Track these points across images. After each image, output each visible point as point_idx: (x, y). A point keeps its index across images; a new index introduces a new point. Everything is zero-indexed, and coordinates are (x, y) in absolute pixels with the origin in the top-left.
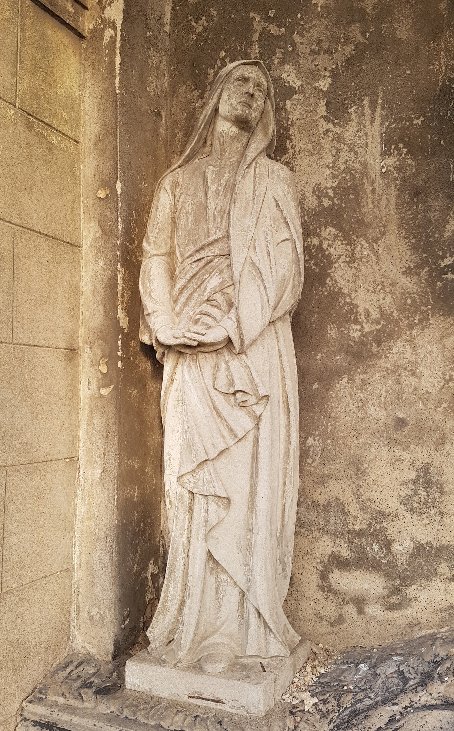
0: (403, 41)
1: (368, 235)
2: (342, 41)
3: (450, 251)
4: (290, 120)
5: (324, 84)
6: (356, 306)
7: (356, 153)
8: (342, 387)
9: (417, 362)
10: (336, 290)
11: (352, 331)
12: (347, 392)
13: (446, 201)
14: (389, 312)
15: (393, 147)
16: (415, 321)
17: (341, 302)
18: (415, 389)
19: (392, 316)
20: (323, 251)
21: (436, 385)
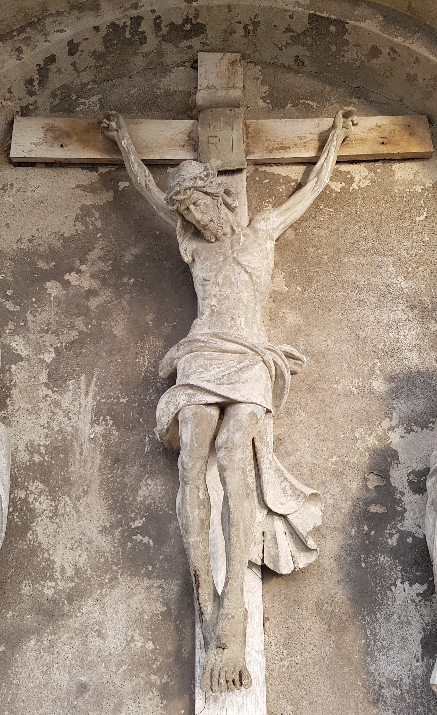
0: (117, 337)
1: (72, 493)
2: (68, 326)
3: (140, 514)
4: (13, 382)
5: (49, 357)
6: (53, 562)
7: (69, 418)
8: (29, 650)
9: (103, 622)
10: (36, 544)
11: (46, 588)
12: (34, 655)
13: (141, 469)
14: (83, 569)
15: (101, 418)
16: (106, 580)
17: (39, 557)
18: (100, 651)
19: (86, 574)
20: (28, 504)
21: (119, 646)
